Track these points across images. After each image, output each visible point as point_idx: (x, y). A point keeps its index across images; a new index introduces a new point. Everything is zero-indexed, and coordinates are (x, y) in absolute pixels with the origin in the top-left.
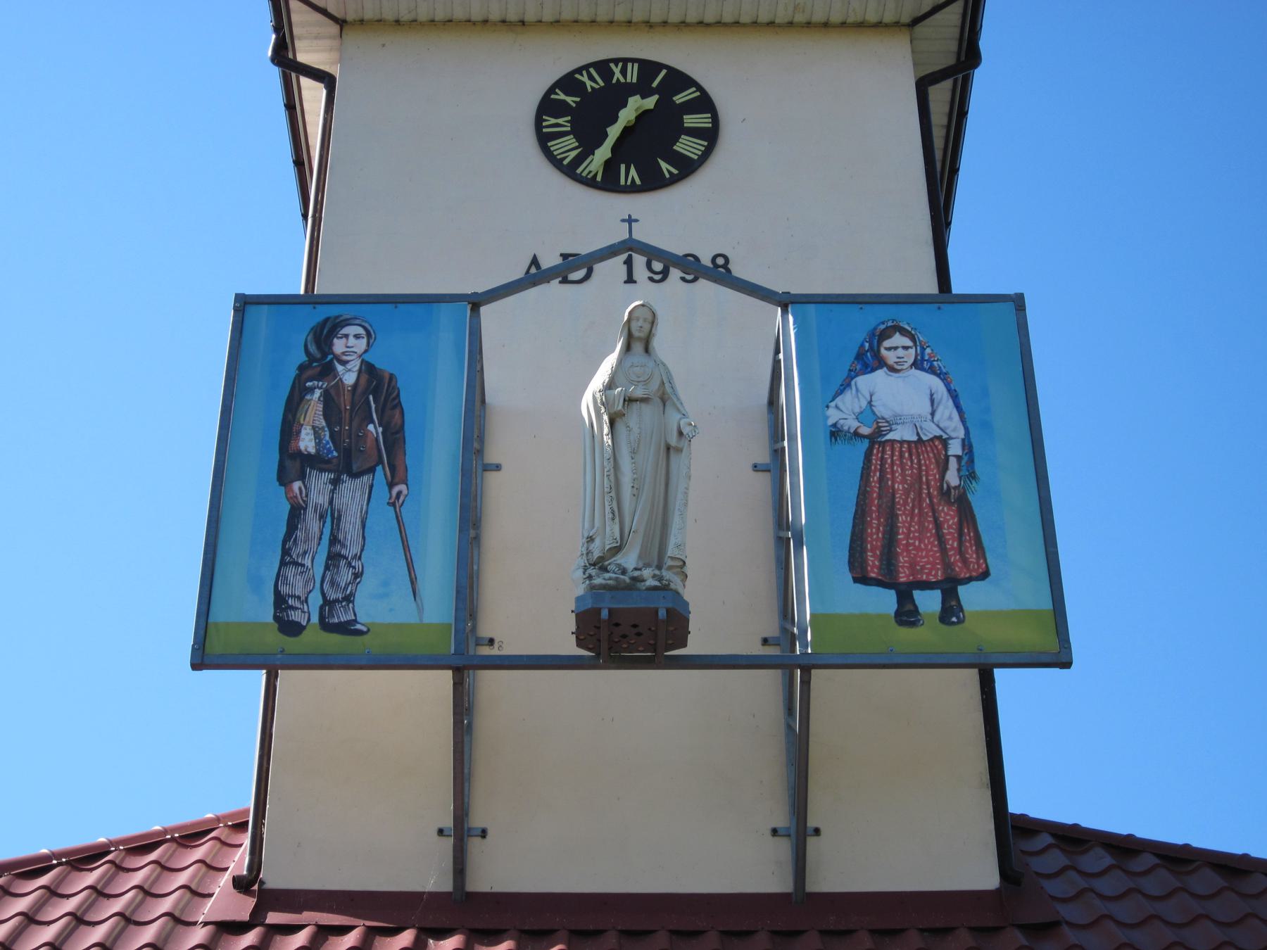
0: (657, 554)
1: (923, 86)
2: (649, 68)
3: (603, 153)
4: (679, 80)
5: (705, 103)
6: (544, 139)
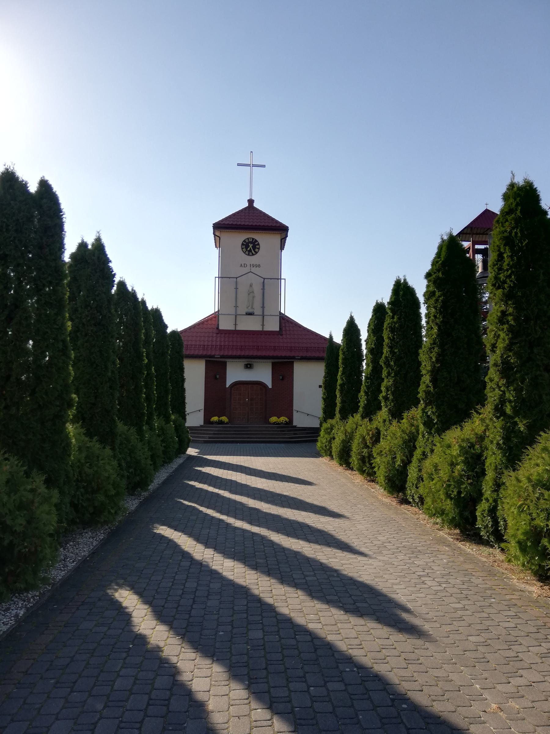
0: (252, 308)
1: (281, 240)
2: (253, 239)
3: (253, 252)
4: (256, 241)
5: (258, 244)
6: (242, 249)
